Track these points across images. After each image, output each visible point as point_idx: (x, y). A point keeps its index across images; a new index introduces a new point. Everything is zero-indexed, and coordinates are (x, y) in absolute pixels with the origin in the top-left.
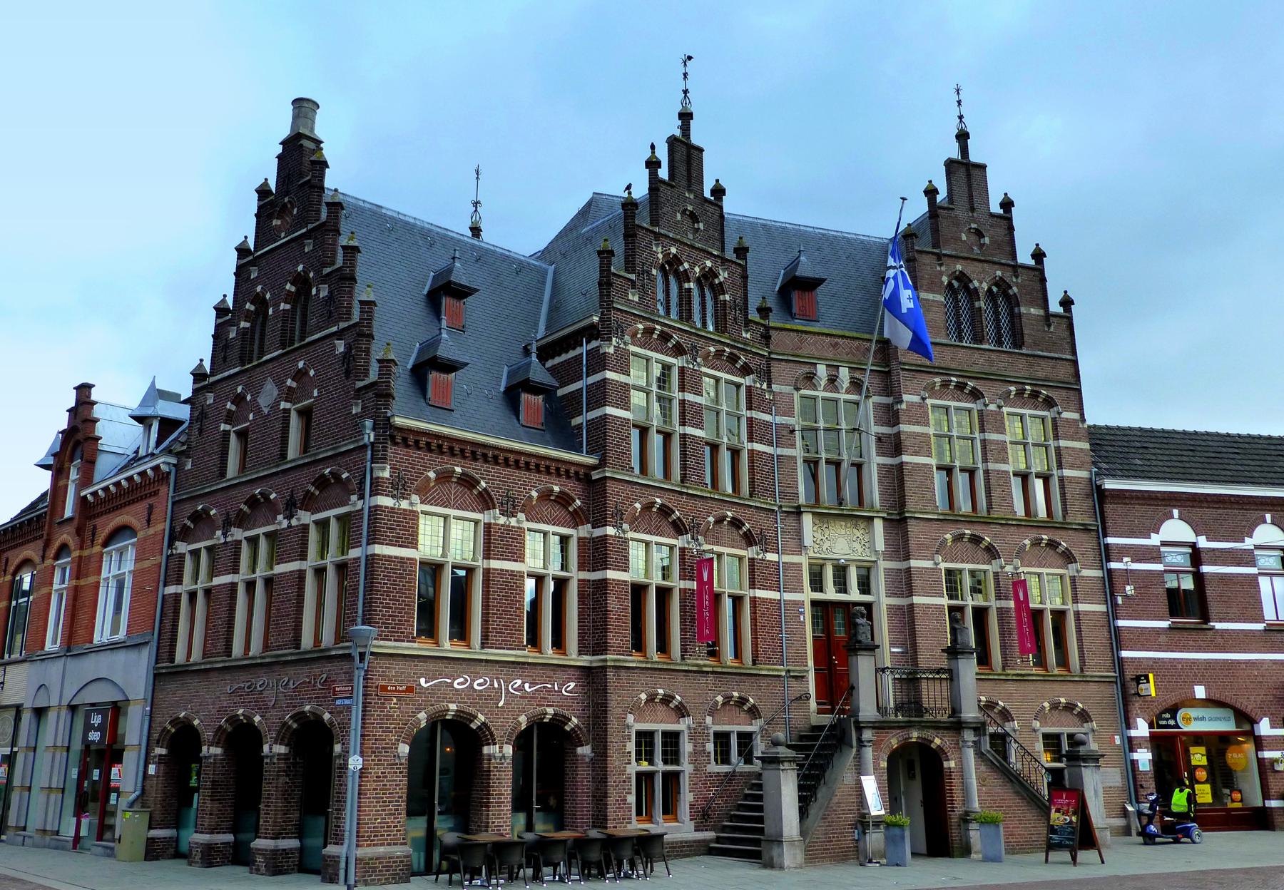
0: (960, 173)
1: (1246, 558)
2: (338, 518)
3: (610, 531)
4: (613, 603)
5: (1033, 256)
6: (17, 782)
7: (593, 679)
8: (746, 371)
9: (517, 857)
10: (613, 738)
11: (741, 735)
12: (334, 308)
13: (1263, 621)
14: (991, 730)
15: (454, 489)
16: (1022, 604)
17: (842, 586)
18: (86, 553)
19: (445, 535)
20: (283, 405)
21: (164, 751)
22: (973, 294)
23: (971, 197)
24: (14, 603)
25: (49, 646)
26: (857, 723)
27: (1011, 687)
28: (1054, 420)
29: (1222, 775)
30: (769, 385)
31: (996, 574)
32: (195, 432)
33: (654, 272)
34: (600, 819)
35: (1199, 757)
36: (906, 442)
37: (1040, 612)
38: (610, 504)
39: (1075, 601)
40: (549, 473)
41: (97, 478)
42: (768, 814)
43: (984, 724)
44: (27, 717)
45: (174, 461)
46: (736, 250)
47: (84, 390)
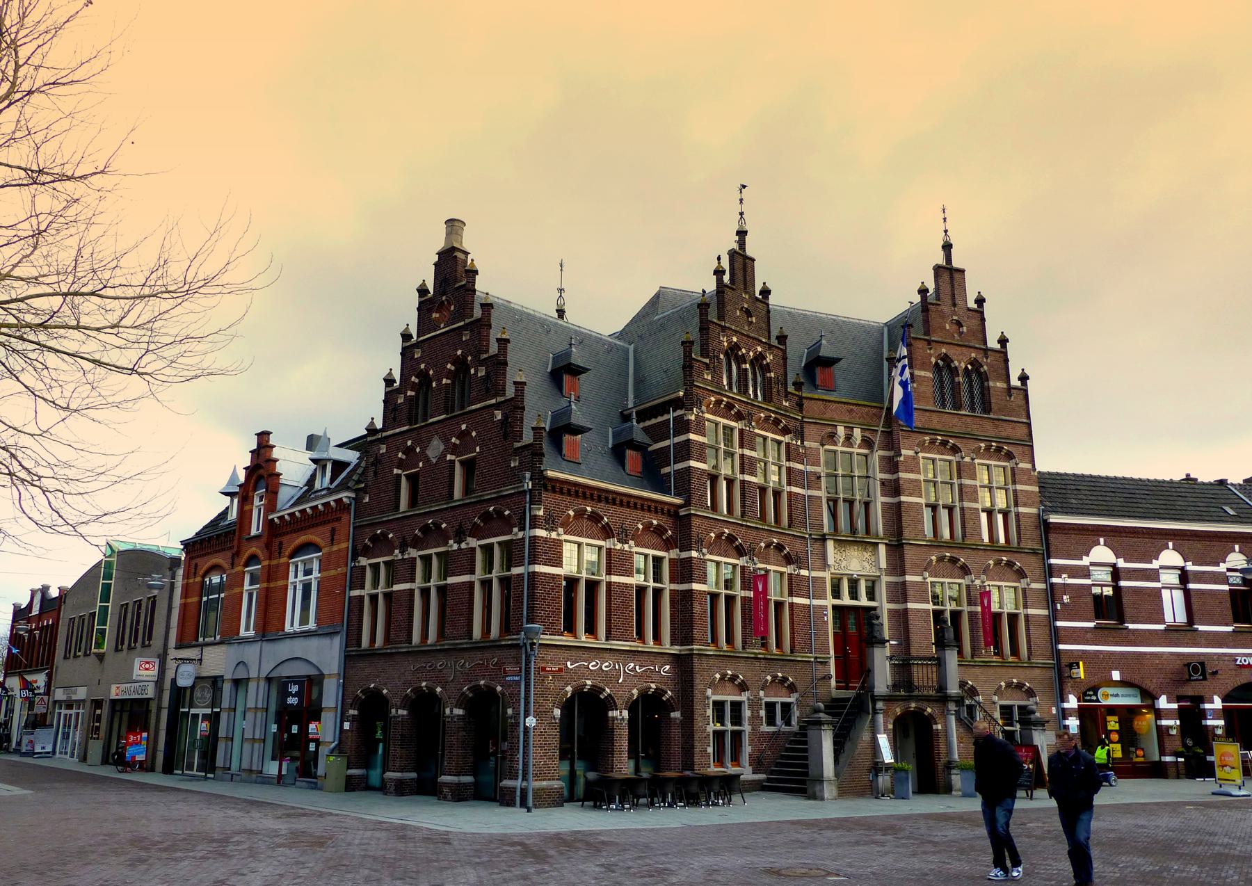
0: (945, 276)
1: (1153, 575)
2: (500, 543)
3: (694, 554)
4: (696, 607)
5: (999, 342)
6: (222, 733)
7: (683, 664)
8: (785, 431)
9: (643, 790)
10: (698, 707)
11: (783, 704)
12: (493, 383)
13: (1164, 623)
14: (967, 702)
15: (586, 523)
16: (987, 609)
17: (854, 595)
18: (274, 562)
19: (577, 556)
20: (449, 457)
21: (356, 712)
22: (954, 371)
23: (953, 295)
24: (205, 599)
25: (242, 633)
26: (873, 696)
27: (977, 671)
28: (1013, 469)
29: (1129, 738)
30: (802, 442)
31: (968, 587)
32: (370, 474)
33: (722, 356)
34: (689, 763)
35: (1113, 724)
36: (904, 486)
37: (999, 615)
38: (694, 534)
39: (1026, 607)
40: (649, 511)
41: (279, 506)
42: (811, 762)
43: (962, 699)
44: (227, 688)
45: (353, 495)
46: (777, 338)
47: (263, 436)
